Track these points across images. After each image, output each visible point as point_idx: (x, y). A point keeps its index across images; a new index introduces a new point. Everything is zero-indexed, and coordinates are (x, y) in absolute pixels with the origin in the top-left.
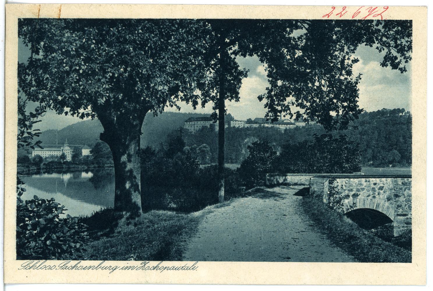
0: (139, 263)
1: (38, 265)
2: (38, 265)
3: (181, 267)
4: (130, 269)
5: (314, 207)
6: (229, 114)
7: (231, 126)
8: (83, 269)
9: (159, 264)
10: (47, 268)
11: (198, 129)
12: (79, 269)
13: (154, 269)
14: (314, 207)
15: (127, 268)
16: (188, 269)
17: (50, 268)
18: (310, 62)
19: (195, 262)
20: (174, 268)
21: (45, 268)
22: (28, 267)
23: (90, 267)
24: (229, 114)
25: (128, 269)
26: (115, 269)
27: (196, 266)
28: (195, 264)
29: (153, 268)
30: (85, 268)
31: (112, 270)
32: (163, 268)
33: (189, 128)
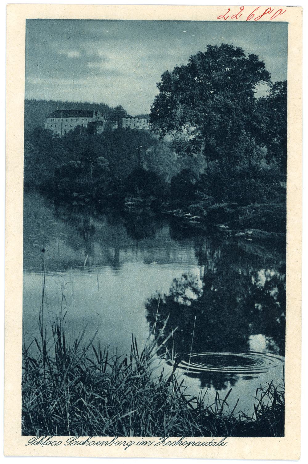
0: (156, 439)
1: (44, 440)
2: (44, 440)
3: (208, 443)
4: (147, 445)
5: (244, 77)
6: (120, 105)
7: (123, 126)
8: (71, 445)
9: (223, 440)
10: (52, 444)
11: (68, 130)
12: (91, 444)
13: (83, 444)
14: (244, 77)
15: (143, 443)
16: (216, 444)
17: (56, 444)
18: (276, 319)
19: (223, 438)
20: (194, 444)
21: (50, 444)
22: (36, 442)
23: (104, 443)
24: (120, 105)
25: (144, 445)
26: (130, 445)
27: (225, 441)
28: (223, 440)
29: (82, 443)
30: (103, 444)
31: (127, 446)
32: (186, 443)
33: (53, 128)
